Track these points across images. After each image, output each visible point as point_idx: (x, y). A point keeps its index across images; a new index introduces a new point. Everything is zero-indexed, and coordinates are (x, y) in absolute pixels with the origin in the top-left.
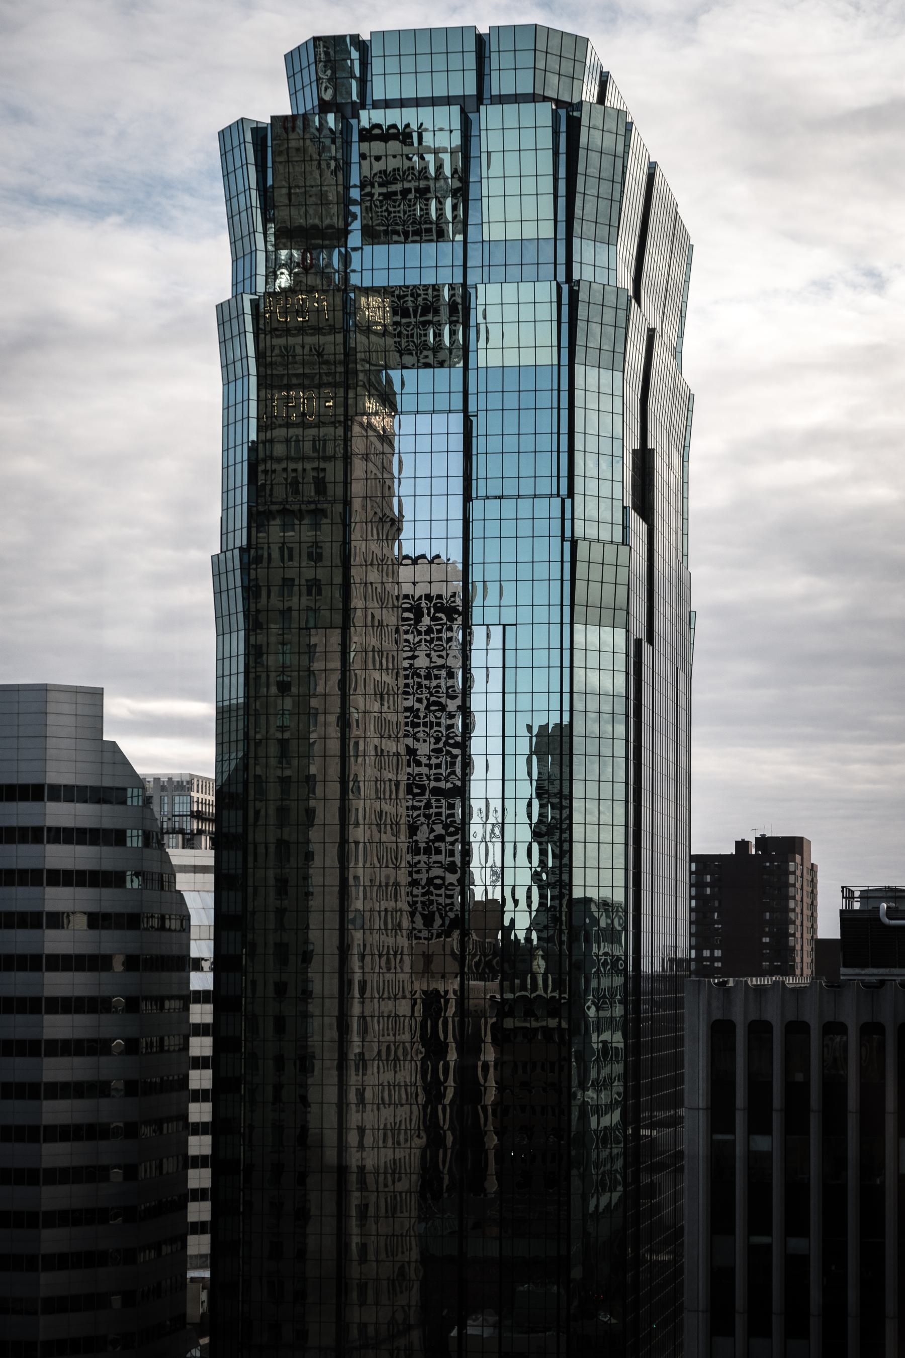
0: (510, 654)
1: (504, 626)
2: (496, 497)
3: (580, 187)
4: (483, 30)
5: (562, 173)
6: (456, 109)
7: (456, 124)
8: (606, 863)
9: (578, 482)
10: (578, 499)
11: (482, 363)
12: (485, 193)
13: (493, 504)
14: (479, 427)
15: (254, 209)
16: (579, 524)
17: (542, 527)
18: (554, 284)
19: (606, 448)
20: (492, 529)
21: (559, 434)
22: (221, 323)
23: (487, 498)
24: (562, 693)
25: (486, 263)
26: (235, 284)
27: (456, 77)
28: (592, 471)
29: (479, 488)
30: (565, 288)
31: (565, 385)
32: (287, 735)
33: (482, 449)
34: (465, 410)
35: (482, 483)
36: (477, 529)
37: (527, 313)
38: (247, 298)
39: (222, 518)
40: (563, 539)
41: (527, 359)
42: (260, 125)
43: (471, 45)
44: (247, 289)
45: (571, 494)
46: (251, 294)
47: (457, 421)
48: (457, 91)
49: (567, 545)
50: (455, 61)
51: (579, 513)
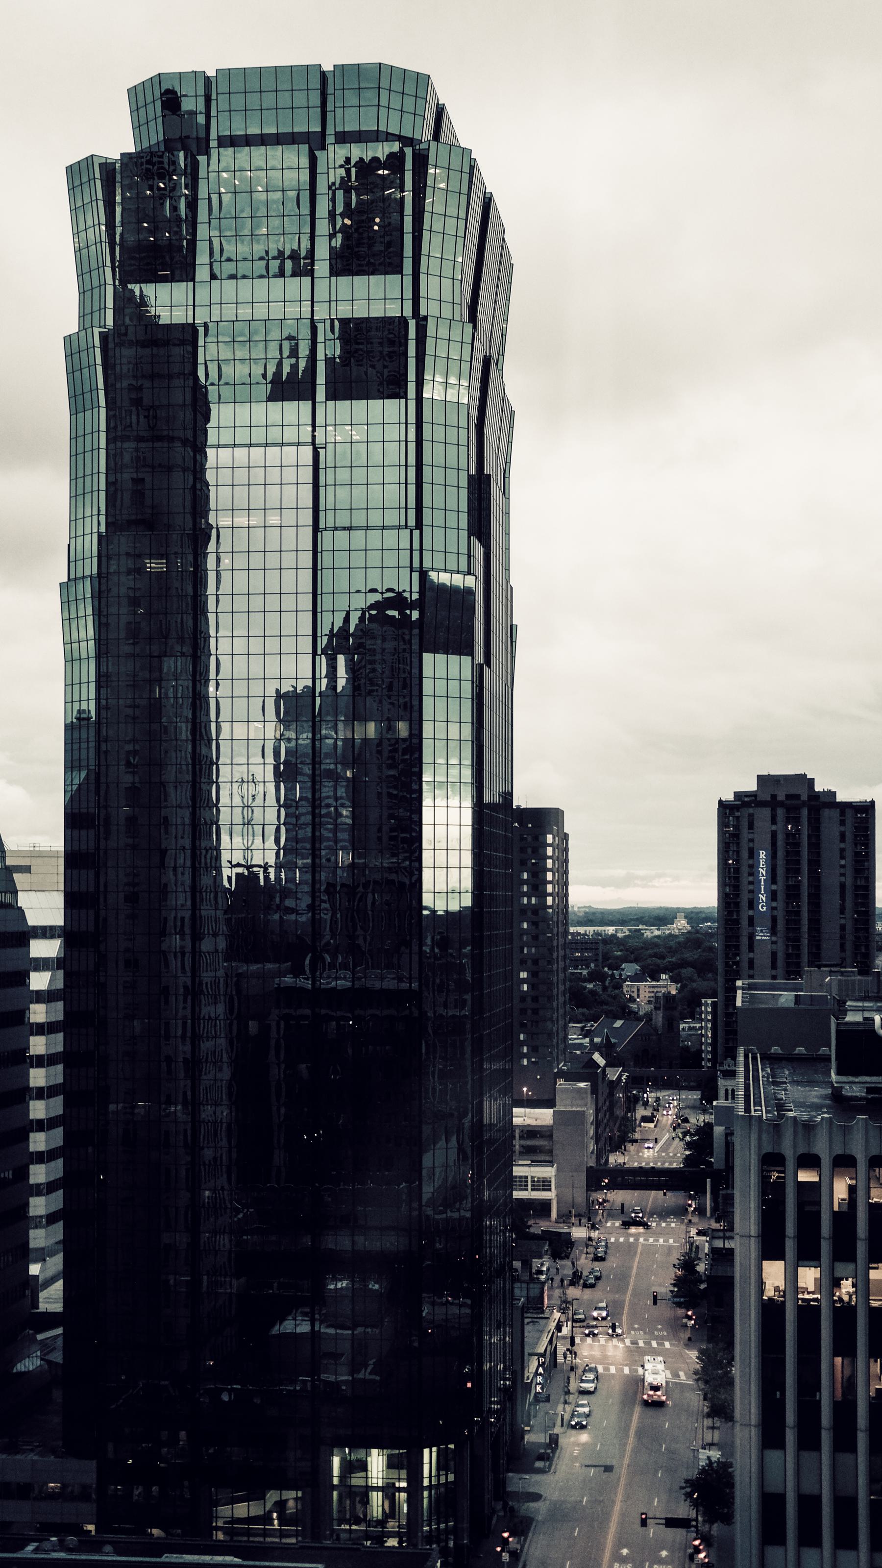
2: (344, 529)
3: (429, 350)
4: (328, 67)
7: (305, 162)
8: (452, 548)
9: (426, 513)
10: (427, 530)
13: (342, 535)
15: (103, 244)
16: (427, 555)
19: (447, 272)
20: (342, 559)
22: (69, 355)
23: (336, 529)
25: (333, 298)
26: (82, 316)
27: (301, 114)
28: (439, 503)
32: (138, 594)
34: (313, 443)
36: (326, 560)
38: (96, 331)
39: (69, 545)
42: (108, 161)
43: (316, 83)
44: (96, 322)
45: (419, 525)
46: (100, 327)
49: (416, 576)
50: (300, 99)
51: (427, 545)
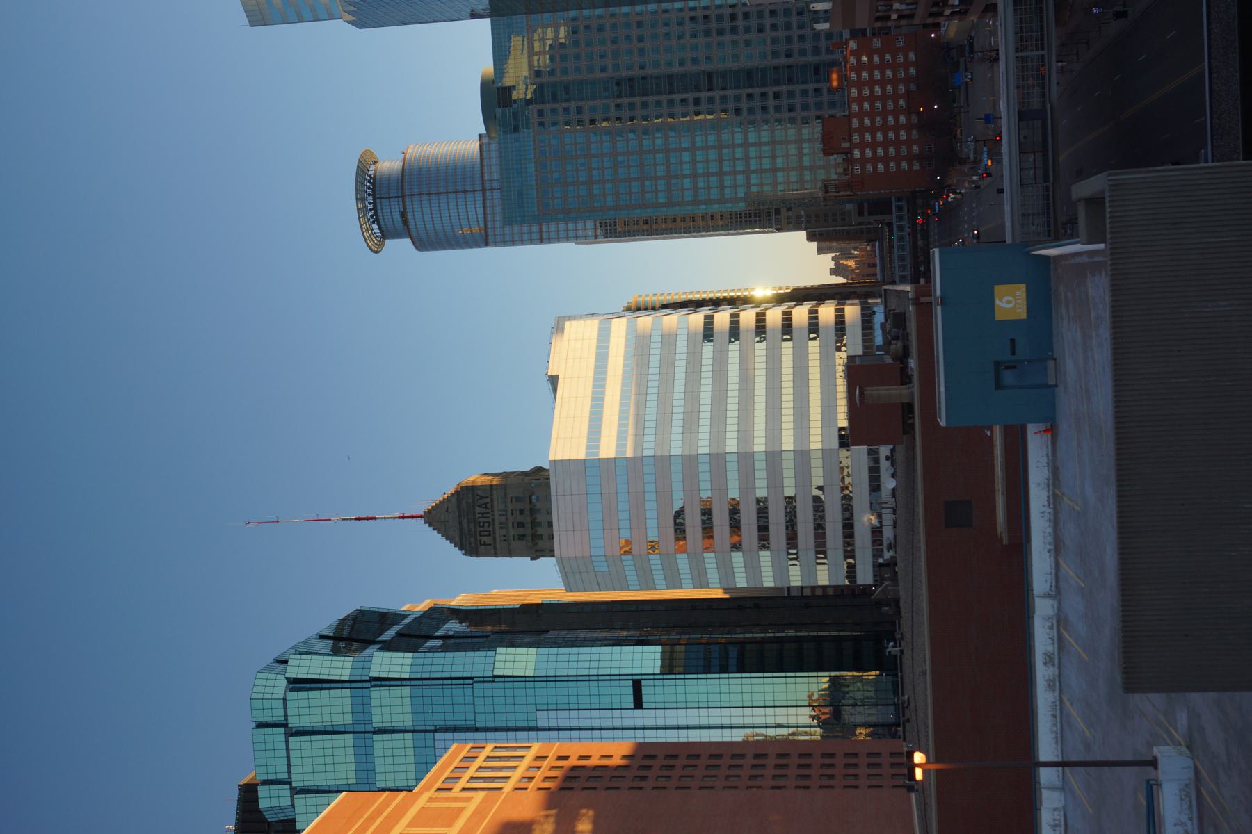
0: (658, 705)
1: (537, 710)
5: (387, 683)
6: (291, 739)
10: (474, 674)
11: (411, 724)
12: (330, 724)
14: (440, 724)
17: (488, 693)
18: (371, 689)
21: (443, 685)
24: (729, 678)
28: (461, 668)
29: (471, 723)
30: (373, 683)
31: (420, 682)
33: (452, 723)
35: (468, 723)
37: (386, 702)
40: (493, 682)
41: (348, 701)
47: (438, 735)
48: (283, 737)
49: (496, 680)
